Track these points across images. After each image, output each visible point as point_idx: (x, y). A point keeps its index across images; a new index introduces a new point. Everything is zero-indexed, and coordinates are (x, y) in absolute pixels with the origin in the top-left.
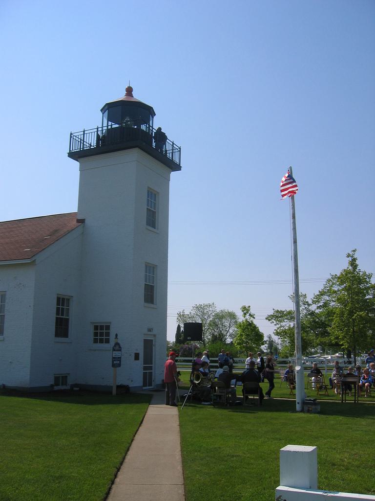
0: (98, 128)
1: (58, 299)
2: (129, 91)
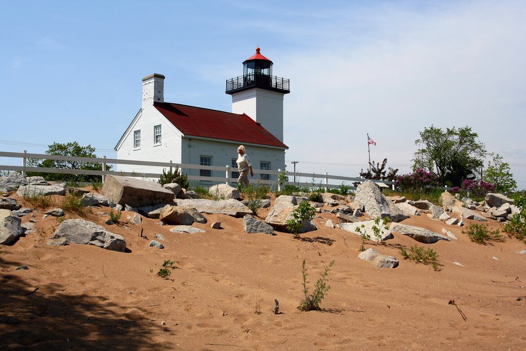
2: (258, 50)
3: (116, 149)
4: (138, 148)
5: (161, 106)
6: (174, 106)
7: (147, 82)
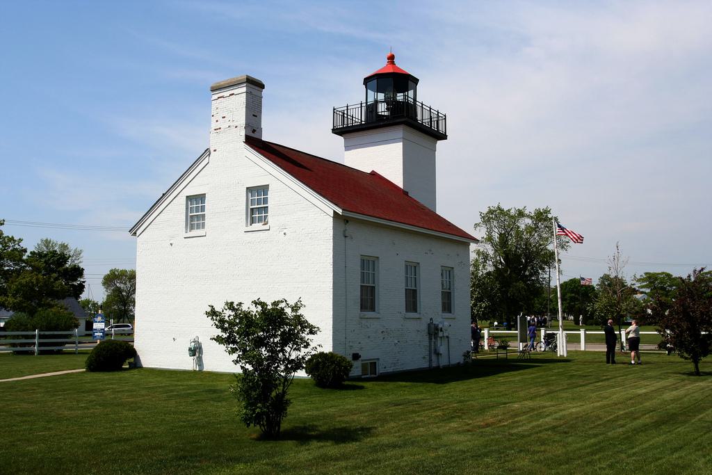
0: (361, 104)
1: (363, 261)
2: (391, 58)
3: (133, 231)
4: (195, 232)
5: (254, 141)
6: (275, 147)
7: (226, 94)
